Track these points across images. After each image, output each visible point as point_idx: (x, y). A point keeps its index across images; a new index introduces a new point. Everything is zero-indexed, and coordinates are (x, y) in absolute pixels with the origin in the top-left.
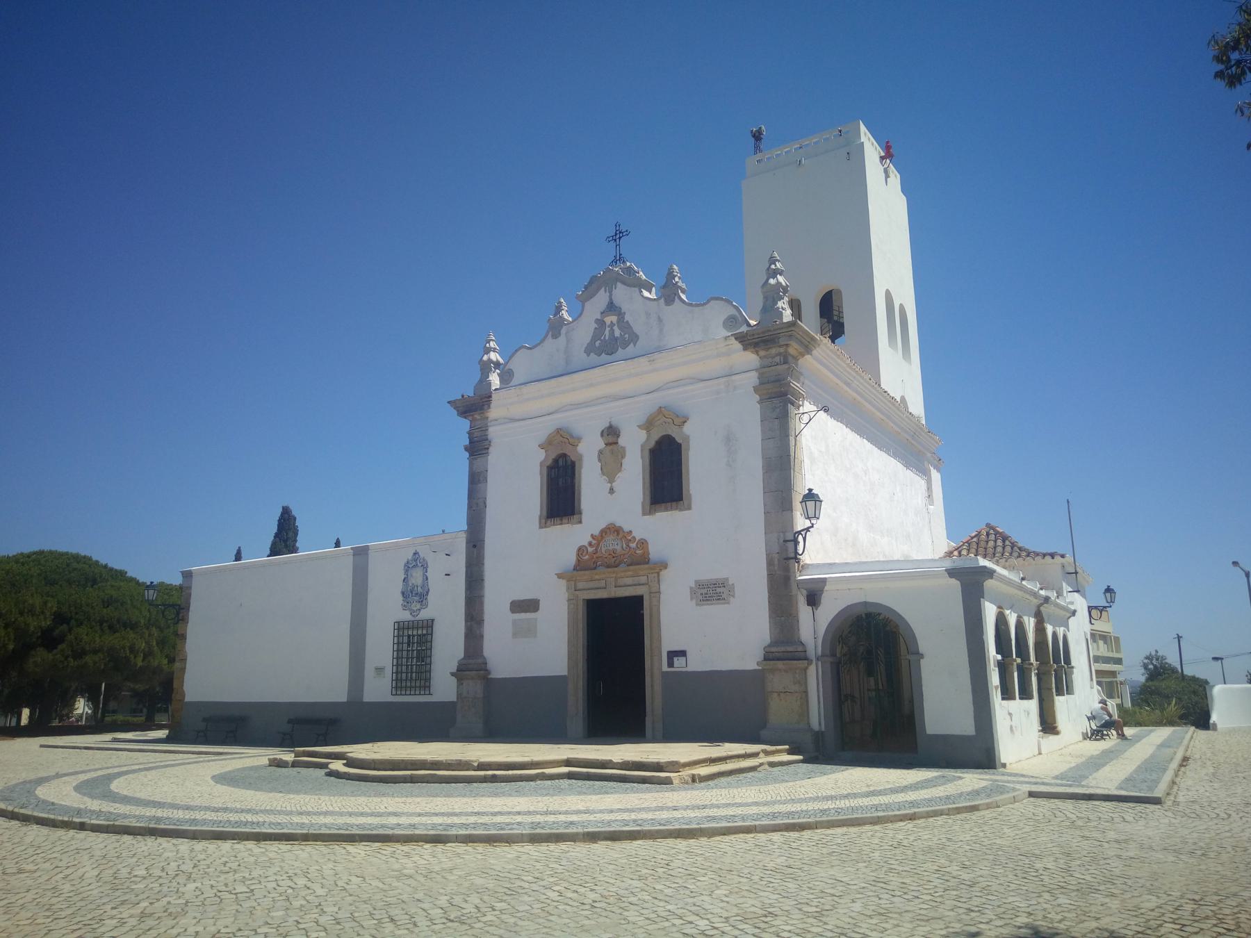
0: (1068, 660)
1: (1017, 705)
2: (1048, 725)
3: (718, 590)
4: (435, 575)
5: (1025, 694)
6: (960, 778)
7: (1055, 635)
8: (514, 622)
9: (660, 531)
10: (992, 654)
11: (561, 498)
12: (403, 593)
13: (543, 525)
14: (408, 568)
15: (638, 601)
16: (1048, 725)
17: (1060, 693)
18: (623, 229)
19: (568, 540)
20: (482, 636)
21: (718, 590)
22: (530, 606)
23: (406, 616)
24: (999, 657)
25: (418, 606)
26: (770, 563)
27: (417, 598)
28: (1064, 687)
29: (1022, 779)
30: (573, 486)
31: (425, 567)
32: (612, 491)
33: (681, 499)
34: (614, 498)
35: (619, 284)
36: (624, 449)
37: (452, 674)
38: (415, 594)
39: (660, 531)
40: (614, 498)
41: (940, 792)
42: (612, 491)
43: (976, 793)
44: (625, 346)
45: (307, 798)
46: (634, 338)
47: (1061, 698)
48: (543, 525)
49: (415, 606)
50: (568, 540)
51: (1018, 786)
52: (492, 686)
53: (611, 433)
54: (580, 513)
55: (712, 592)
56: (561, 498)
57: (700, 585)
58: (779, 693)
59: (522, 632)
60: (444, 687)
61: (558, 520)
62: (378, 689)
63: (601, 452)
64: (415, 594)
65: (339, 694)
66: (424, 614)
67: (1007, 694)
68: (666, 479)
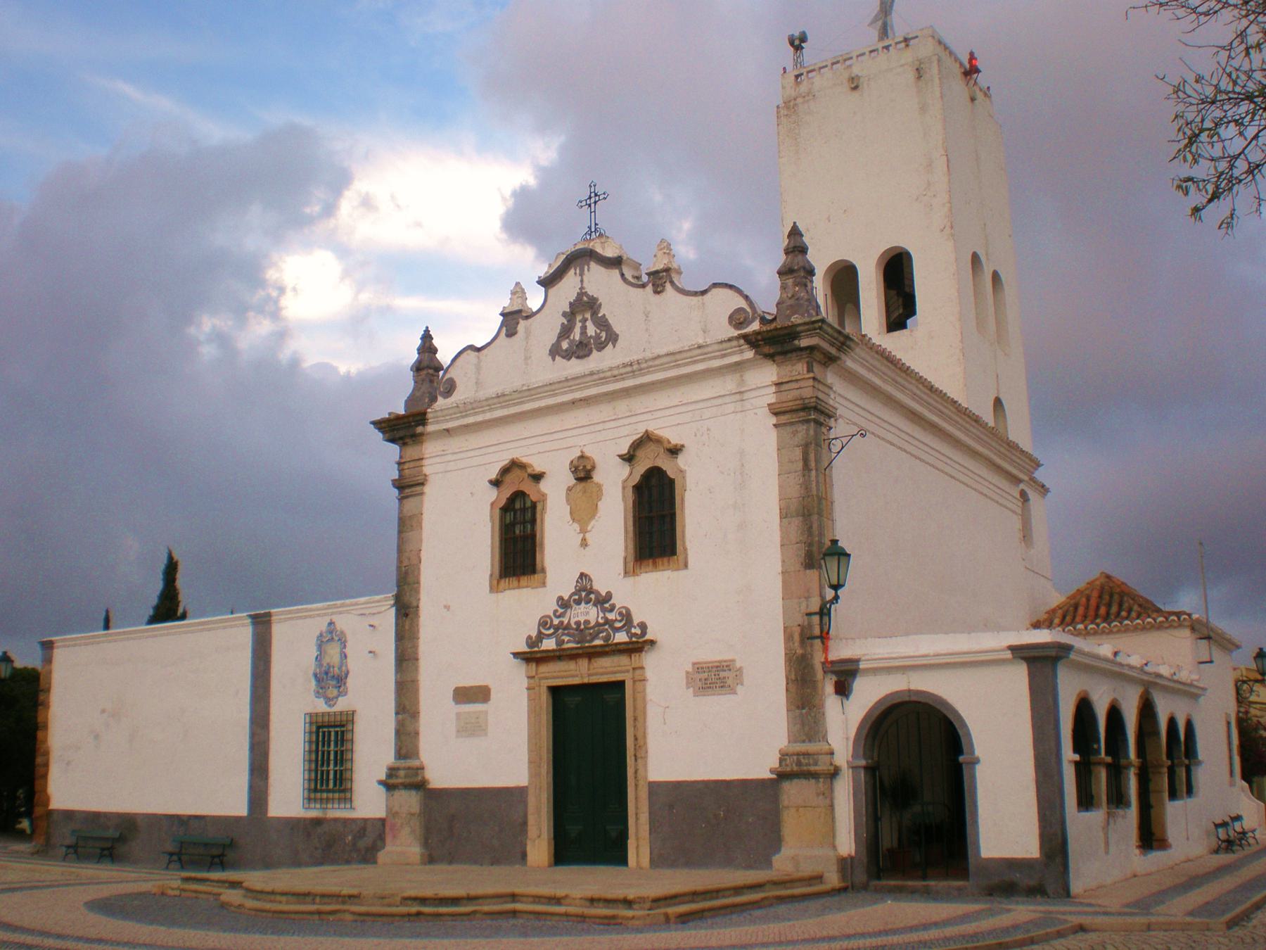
0: (1191, 751)
1: (1096, 816)
2: (1150, 837)
3: (722, 674)
4: (356, 664)
5: (1117, 799)
6: (1009, 911)
7: (1172, 722)
8: (458, 715)
9: (647, 597)
10: (1069, 755)
11: (518, 553)
12: (315, 675)
13: (494, 589)
14: (321, 643)
15: (620, 685)
16: (1150, 837)
17: (1173, 795)
18: (600, 190)
19: (527, 608)
20: (417, 733)
21: (722, 674)
22: (480, 694)
23: (321, 706)
24: (1077, 757)
25: (335, 692)
26: (788, 637)
27: (334, 683)
28: (1182, 787)
29: (1086, 909)
30: (533, 536)
31: (344, 644)
32: (584, 543)
33: (673, 552)
34: (586, 545)
35: (593, 265)
36: (599, 486)
37: (381, 782)
38: (331, 679)
39: (647, 597)
40: (586, 545)
41: (986, 924)
42: (584, 543)
43: (1035, 923)
44: (601, 347)
45: (192, 932)
46: (613, 338)
47: (1178, 803)
48: (494, 589)
49: (333, 692)
50: (527, 608)
51: (1069, 918)
52: (434, 798)
53: (583, 472)
54: (543, 570)
55: (714, 678)
56: (518, 553)
57: (699, 667)
58: (797, 808)
59: (471, 729)
60: (368, 799)
61: (514, 581)
62: (288, 798)
63: (570, 489)
64: (331, 679)
65: (235, 805)
66: (342, 705)
67: (1086, 801)
68: (656, 526)
